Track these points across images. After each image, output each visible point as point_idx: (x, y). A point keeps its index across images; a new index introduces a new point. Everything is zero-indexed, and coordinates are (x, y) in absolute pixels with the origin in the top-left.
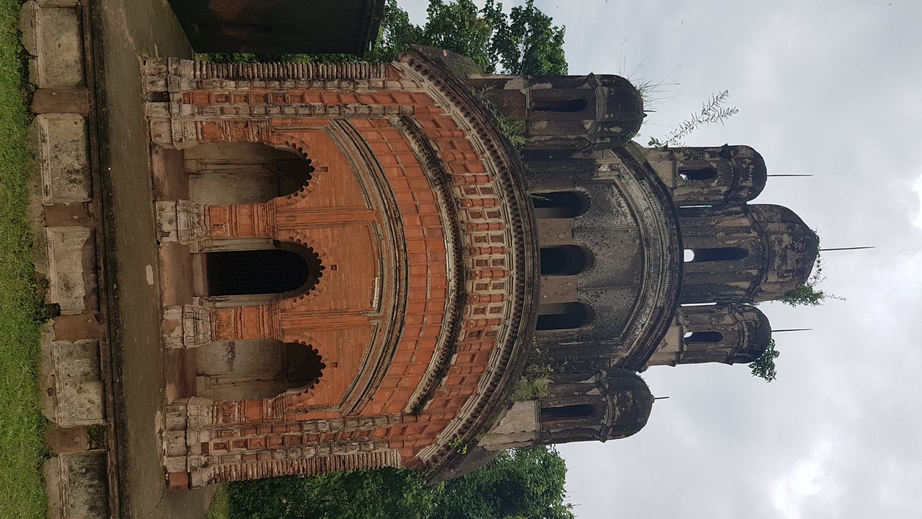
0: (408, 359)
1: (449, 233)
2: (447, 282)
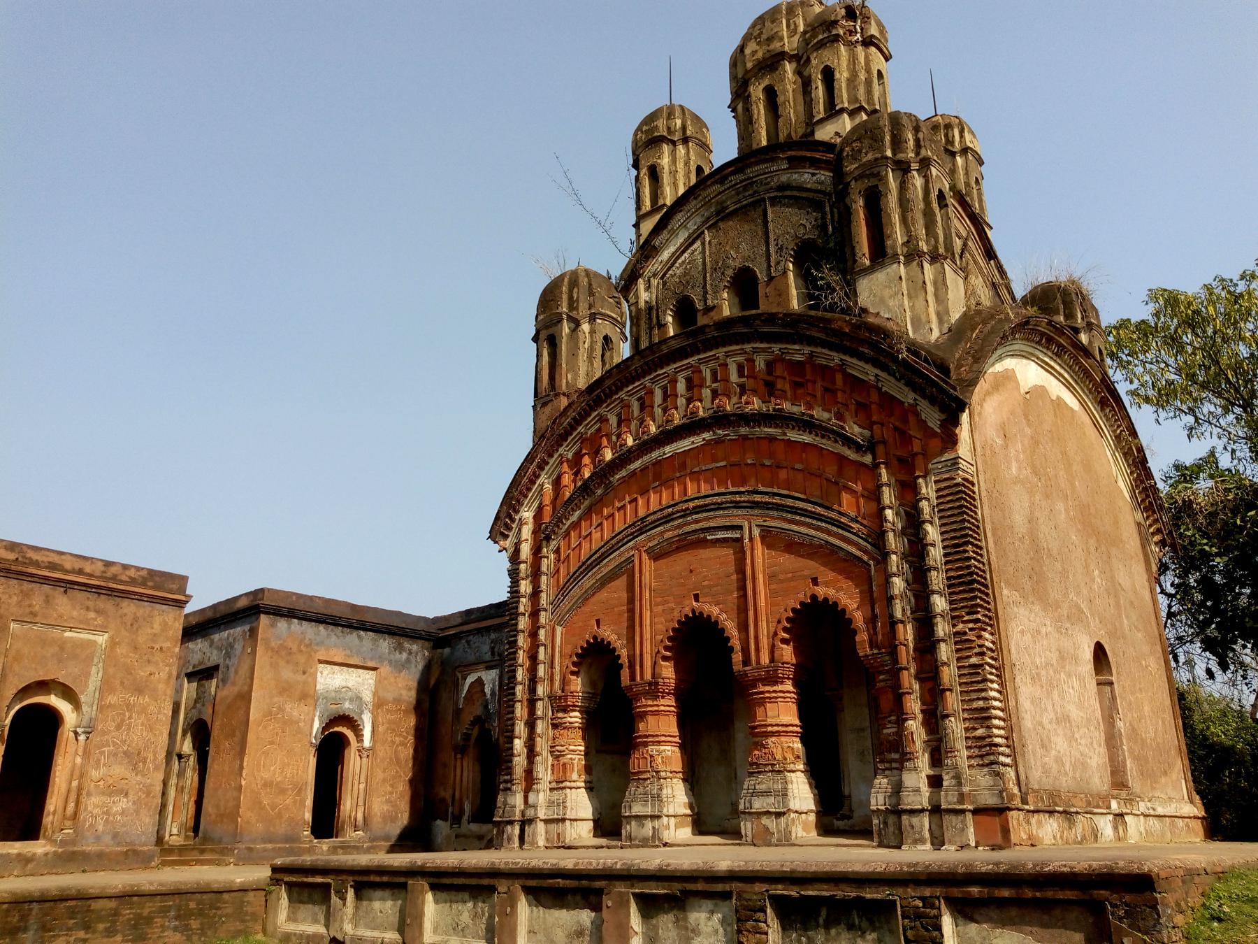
0: (800, 476)
1: (655, 455)
2: (708, 443)
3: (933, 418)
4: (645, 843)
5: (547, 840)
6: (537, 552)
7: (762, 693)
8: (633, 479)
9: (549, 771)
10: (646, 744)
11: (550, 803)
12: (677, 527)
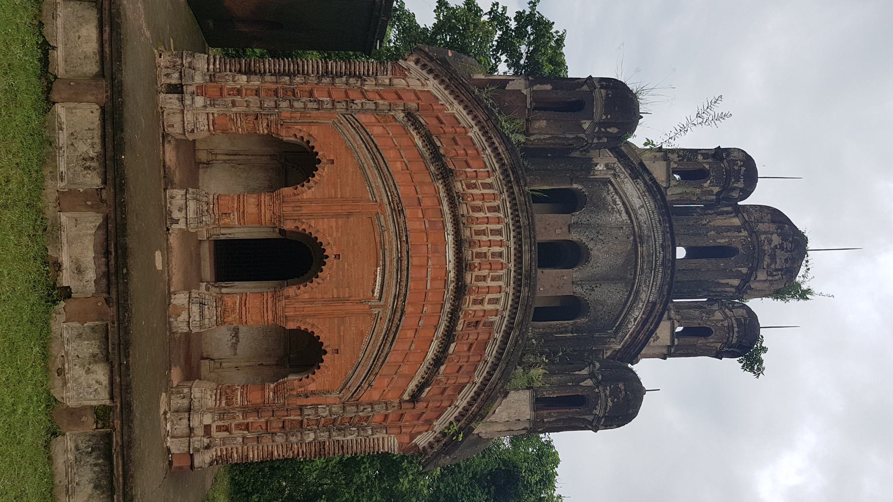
1: (449, 226)
2: (447, 273)
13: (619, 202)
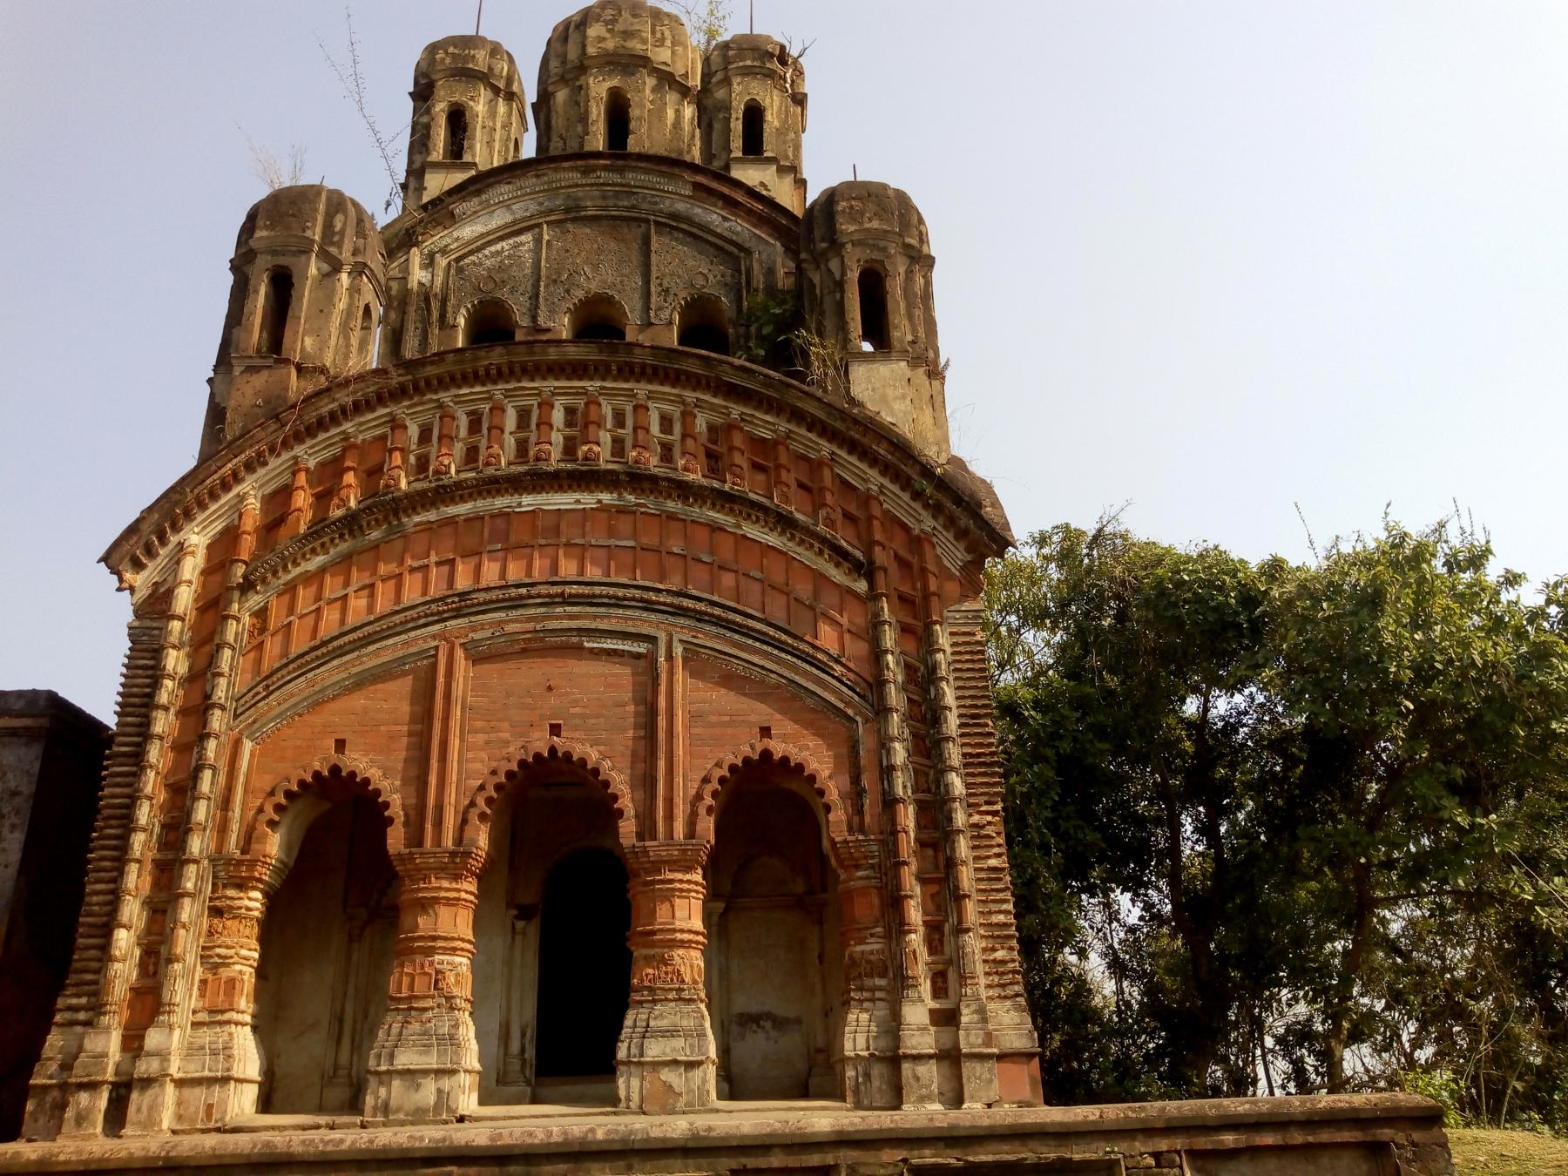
1: (501, 502)
2: (603, 508)
3: (951, 554)
4: (419, 1116)
5: (180, 1118)
6: (213, 607)
7: (671, 881)
8: (448, 530)
9: (195, 992)
10: (430, 952)
11: (192, 1051)
12: (529, 619)
13: (499, 247)
